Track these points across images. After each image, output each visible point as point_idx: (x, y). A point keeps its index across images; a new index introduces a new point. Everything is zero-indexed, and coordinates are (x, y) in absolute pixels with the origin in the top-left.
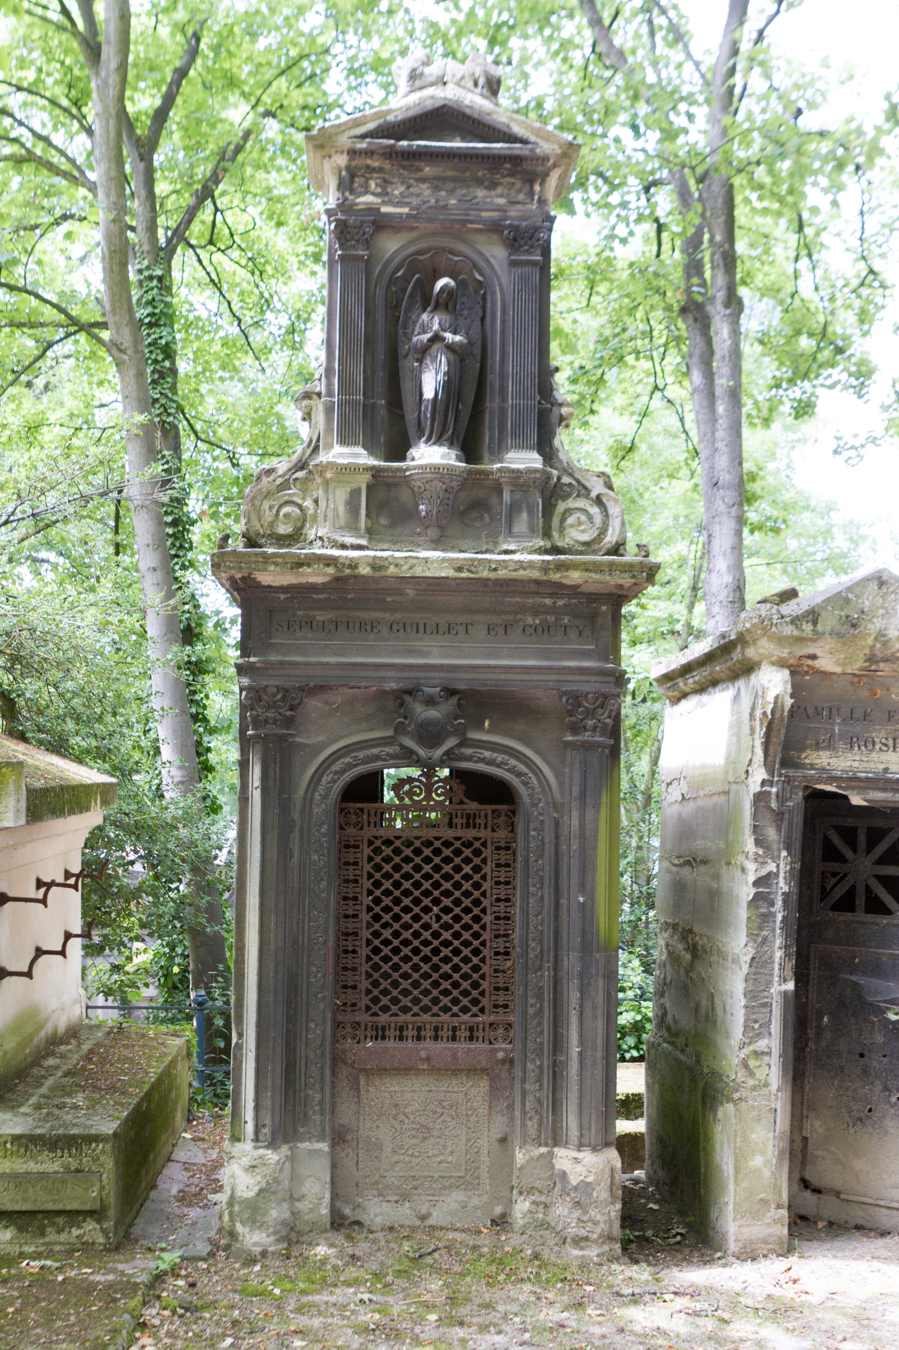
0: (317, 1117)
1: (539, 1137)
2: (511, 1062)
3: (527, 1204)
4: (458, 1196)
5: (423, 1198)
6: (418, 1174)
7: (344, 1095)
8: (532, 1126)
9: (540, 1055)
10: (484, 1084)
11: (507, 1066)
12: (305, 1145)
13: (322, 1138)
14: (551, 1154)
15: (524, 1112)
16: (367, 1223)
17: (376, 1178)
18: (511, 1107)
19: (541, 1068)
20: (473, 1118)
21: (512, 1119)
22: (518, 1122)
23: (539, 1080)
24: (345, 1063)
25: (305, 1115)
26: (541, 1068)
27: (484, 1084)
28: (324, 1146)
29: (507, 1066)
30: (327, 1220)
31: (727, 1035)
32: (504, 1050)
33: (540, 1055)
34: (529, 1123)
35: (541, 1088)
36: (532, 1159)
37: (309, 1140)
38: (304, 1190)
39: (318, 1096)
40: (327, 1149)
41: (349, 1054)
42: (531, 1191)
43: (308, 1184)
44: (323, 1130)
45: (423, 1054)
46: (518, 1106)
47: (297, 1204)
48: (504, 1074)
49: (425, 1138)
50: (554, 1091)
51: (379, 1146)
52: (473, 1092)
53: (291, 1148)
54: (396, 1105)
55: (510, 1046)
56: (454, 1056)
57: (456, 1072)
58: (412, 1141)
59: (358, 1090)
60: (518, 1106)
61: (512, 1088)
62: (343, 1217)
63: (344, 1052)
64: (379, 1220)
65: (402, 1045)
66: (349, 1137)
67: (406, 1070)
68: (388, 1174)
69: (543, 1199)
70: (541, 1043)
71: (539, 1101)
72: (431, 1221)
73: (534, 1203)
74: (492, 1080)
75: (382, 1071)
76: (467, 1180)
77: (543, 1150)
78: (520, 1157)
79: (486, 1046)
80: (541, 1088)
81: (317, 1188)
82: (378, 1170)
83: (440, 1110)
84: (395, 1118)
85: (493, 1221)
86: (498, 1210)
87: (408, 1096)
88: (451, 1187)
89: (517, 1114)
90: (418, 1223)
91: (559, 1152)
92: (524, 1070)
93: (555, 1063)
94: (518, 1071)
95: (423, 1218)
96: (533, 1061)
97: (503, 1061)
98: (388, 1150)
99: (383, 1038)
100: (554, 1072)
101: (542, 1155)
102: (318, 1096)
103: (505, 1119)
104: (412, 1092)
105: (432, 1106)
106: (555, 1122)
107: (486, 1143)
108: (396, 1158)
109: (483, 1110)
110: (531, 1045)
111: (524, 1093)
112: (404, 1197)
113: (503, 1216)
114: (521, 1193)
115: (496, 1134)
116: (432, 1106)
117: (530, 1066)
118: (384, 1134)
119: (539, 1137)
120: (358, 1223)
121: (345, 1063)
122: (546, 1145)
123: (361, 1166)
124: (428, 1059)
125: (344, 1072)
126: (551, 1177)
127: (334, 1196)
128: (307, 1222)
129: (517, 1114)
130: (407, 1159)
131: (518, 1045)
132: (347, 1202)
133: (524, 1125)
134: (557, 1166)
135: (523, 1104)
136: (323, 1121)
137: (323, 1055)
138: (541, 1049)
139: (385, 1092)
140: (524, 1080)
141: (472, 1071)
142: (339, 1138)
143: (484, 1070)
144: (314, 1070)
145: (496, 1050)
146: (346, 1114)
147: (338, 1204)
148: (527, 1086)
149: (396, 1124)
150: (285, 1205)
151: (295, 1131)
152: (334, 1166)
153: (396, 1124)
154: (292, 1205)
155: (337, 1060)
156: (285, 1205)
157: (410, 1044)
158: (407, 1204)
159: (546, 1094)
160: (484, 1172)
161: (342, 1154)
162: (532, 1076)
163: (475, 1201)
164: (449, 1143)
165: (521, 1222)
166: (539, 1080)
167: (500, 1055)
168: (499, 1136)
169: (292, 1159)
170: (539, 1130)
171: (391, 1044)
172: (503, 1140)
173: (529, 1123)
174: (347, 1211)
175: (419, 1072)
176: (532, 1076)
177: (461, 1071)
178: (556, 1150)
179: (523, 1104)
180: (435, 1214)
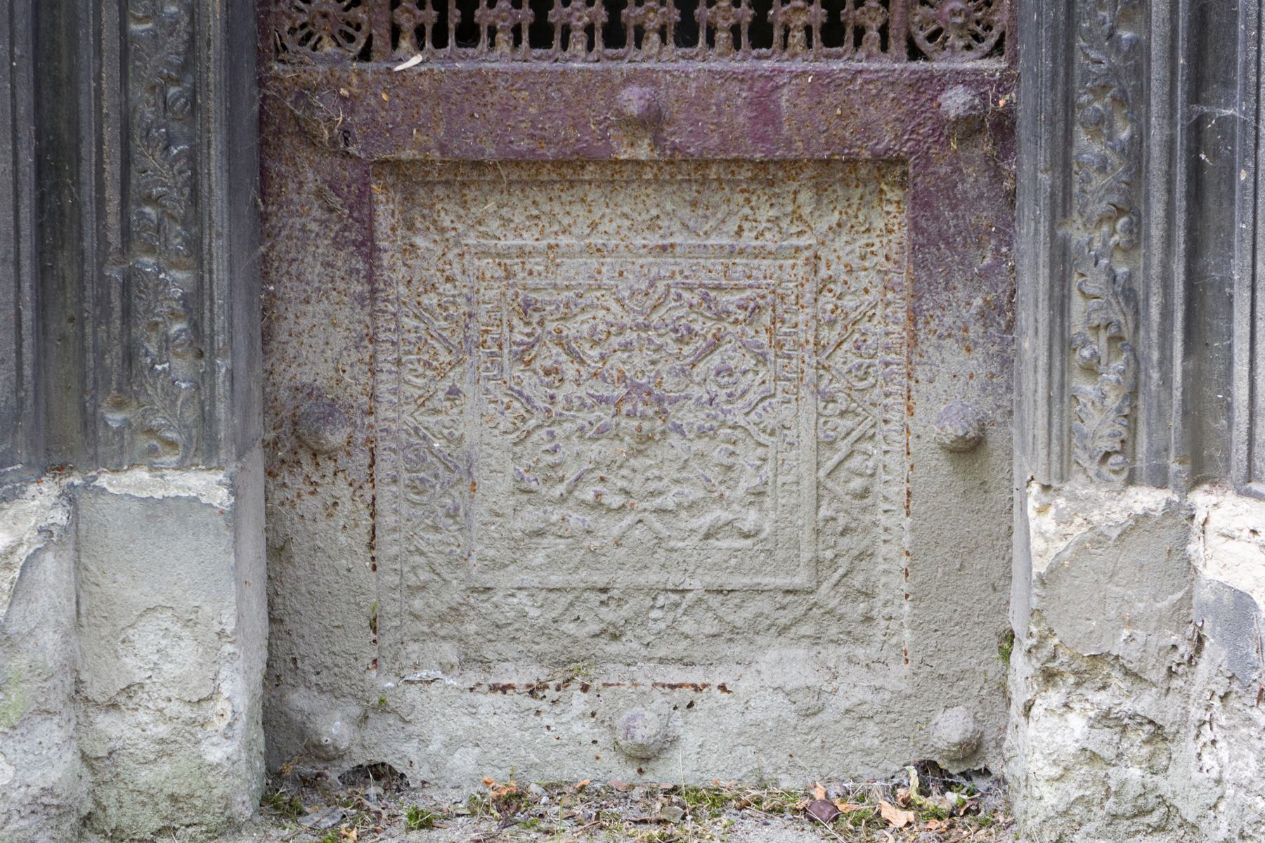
0: (181, 367)
1: (1126, 446)
2: (1003, 128)
3: (1077, 723)
4: (786, 665)
5: (645, 673)
6: (623, 579)
7: (313, 271)
8: (1097, 397)
9: (1132, 100)
10: (888, 222)
11: (986, 146)
12: (132, 482)
13: (202, 448)
14: (1181, 520)
15: (1061, 343)
16: (417, 774)
17: (454, 595)
18: (1001, 315)
19: (1135, 153)
20: (844, 359)
21: (1007, 362)
22: (1034, 383)
23: (1129, 208)
24: (309, 138)
25: (130, 356)
26: (1135, 153)
27: (888, 222)
28: (206, 485)
29: (986, 146)
30: (242, 792)
31: (31, 287)
32: (974, 81)
33: (1132, 100)
34: (1086, 388)
35: (1136, 237)
36: (1099, 539)
37: (149, 459)
38: (133, 666)
39: (179, 279)
40: (221, 497)
41: (323, 104)
42: (1094, 668)
43: (147, 638)
44: (206, 419)
45: (633, 100)
46: (1033, 316)
47: (105, 723)
48: (973, 179)
49: (645, 439)
50: (1194, 251)
51: (463, 470)
52: (844, 249)
53: (70, 498)
54: (527, 308)
55: (995, 66)
56: (764, 107)
57: (770, 173)
58: (594, 450)
59: (368, 248)
60: (1033, 316)
61: (1005, 234)
62: (321, 753)
63: (304, 92)
64: (464, 762)
65: (540, 63)
66: (335, 437)
67: (564, 167)
68: (503, 580)
69: (1145, 703)
70: (1139, 49)
71: (1130, 296)
72: (678, 769)
73: (1105, 718)
74: (921, 203)
75: (467, 173)
76: (822, 605)
77: (1147, 499)
78: (1046, 528)
79: (895, 64)
80: (1136, 237)
81: (185, 657)
82: (459, 562)
83: (705, 327)
84: (523, 356)
85: (926, 767)
86: (951, 728)
87: (574, 269)
88: (754, 628)
89: (1032, 345)
90: (622, 774)
91: (1217, 507)
92: (1064, 163)
93: (1196, 129)
94: (1032, 167)
95: (643, 757)
96: (1100, 124)
97: (969, 127)
98: (497, 487)
99: (468, 35)
100: (1196, 171)
101: (1141, 520)
102: (179, 279)
103: (975, 362)
104: (596, 257)
105: (671, 312)
106: (1194, 382)
107: (898, 456)
108: (531, 517)
109: (885, 327)
110: (1092, 57)
111: (1062, 260)
112: (570, 671)
113: (972, 749)
114: (1049, 676)
115: (942, 418)
116: (671, 312)
117: (1087, 146)
118: (477, 419)
119: (1126, 446)
120: (379, 772)
121: (309, 138)
122: (1160, 479)
123: (389, 547)
124: (651, 122)
125: (306, 176)
126: (1181, 614)
127: (277, 676)
128: (148, 797)
129: (1032, 345)
130: (577, 519)
131: (1035, 55)
132: (333, 691)
133: (1060, 395)
134: (1210, 572)
135: (1060, 307)
136: (202, 381)
137: (194, 107)
138: (1140, 72)
139: (469, 254)
140: (1062, 204)
141: (839, 170)
142: (294, 440)
143: (886, 163)
144: (159, 170)
145: (941, 82)
146: (320, 343)
147: (299, 700)
148: (1077, 233)
149: (530, 383)
150: (51, 733)
151: (89, 422)
152: (277, 551)
153: (530, 383)
154: (82, 726)
155: (271, 133)
156: (51, 733)
157: (579, 61)
158: (579, 701)
159: (1160, 263)
160: (889, 573)
161: (310, 504)
162: (1097, 190)
163: (854, 690)
164: (748, 456)
165: (1051, 798)
166: (1129, 208)
167: (956, 101)
168: (953, 430)
169: (73, 539)
170: (1131, 420)
171: (498, 59)
172: (969, 449)
173: (1086, 388)
174: (335, 728)
175: (618, 174)
176: (1097, 190)
177: (791, 166)
178: (1201, 499)
179: (1060, 307)
180: (690, 739)
